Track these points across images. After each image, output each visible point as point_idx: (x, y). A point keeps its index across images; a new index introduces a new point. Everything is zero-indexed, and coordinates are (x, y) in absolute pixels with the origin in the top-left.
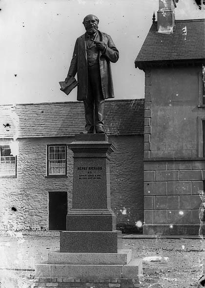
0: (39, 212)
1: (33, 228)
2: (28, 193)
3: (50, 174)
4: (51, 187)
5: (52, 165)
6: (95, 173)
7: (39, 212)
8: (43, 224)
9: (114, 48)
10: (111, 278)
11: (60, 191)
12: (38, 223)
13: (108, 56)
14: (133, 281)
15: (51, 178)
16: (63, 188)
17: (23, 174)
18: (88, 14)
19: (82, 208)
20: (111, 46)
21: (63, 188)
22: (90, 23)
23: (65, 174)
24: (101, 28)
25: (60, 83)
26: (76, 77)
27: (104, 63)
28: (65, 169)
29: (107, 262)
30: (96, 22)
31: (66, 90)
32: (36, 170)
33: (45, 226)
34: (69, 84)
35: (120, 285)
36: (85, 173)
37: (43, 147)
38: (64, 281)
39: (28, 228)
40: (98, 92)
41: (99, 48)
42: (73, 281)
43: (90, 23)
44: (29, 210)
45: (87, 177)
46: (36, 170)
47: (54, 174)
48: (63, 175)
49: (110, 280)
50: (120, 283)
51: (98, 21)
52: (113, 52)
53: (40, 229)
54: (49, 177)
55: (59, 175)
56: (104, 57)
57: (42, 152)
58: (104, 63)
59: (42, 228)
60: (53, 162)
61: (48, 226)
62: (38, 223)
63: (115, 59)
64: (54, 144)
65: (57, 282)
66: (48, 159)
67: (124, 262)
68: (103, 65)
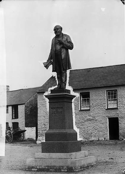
0: (103, 130)
1: (100, 139)
2: (96, 119)
3: (108, 108)
4: (109, 115)
5: (109, 102)
6: (60, 110)
7: (103, 130)
8: (105, 136)
9: (71, 43)
10: (63, 167)
11: (114, 117)
12: (102, 136)
13: (66, 47)
14: (73, 168)
15: (109, 109)
16: (116, 115)
17: (93, 108)
18: (56, 25)
19: (53, 129)
20: (68, 41)
21: (116, 115)
22: (58, 30)
23: (117, 107)
24: (64, 32)
25: (43, 63)
26: (52, 60)
27: (64, 51)
28: (117, 104)
29: (62, 158)
30: (60, 29)
31: (47, 66)
32: (101, 105)
33: (106, 138)
34: (47, 64)
35: (67, 170)
36: (54, 110)
37: (104, 92)
38: (40, 168)
39: (97, 139)
40: (62, 67)
41: (61, 43)
42: (44, 168)
43: (58, 30)
44: (98, 128)
45: (56, 112)
46: (101, 105)
47: (111, 107)
48: (116, 108)
49: (62, 168)
50: (67, 169)
51: (61, 28)
52: (69, 45)
53: (104, 140)
54: (108, 109)
55: (114, 108)
56: (63, 47)
57: (103, 95)
58: (64, 51)
59: (105, 139)
60: (112, 100)
61: (109, 138)
62: (102, 136)
63: (71, 48)
64: (110, 89)
65: (36, 168)
66: (107, 99)
67: (71, 158)
68: (64, 51)
